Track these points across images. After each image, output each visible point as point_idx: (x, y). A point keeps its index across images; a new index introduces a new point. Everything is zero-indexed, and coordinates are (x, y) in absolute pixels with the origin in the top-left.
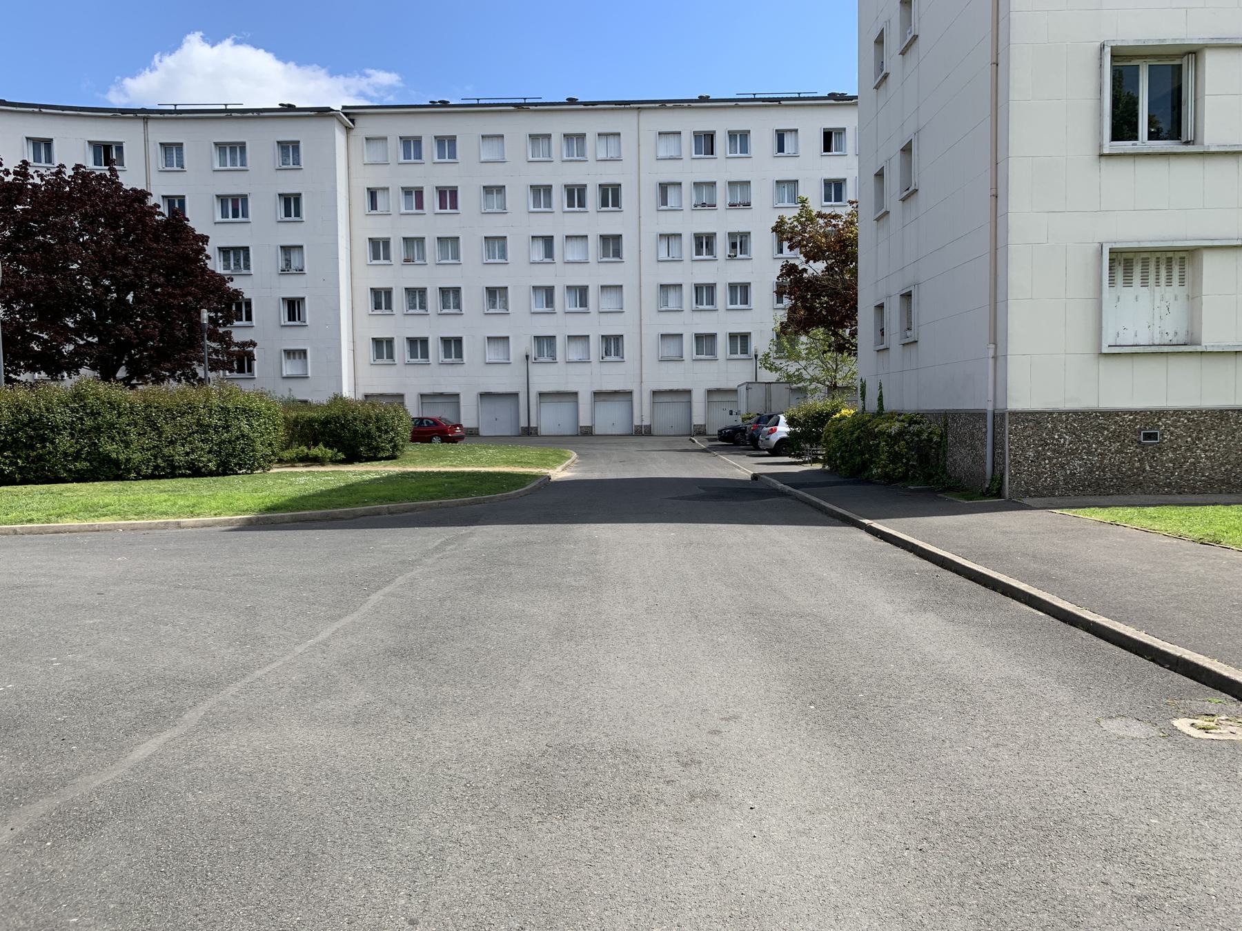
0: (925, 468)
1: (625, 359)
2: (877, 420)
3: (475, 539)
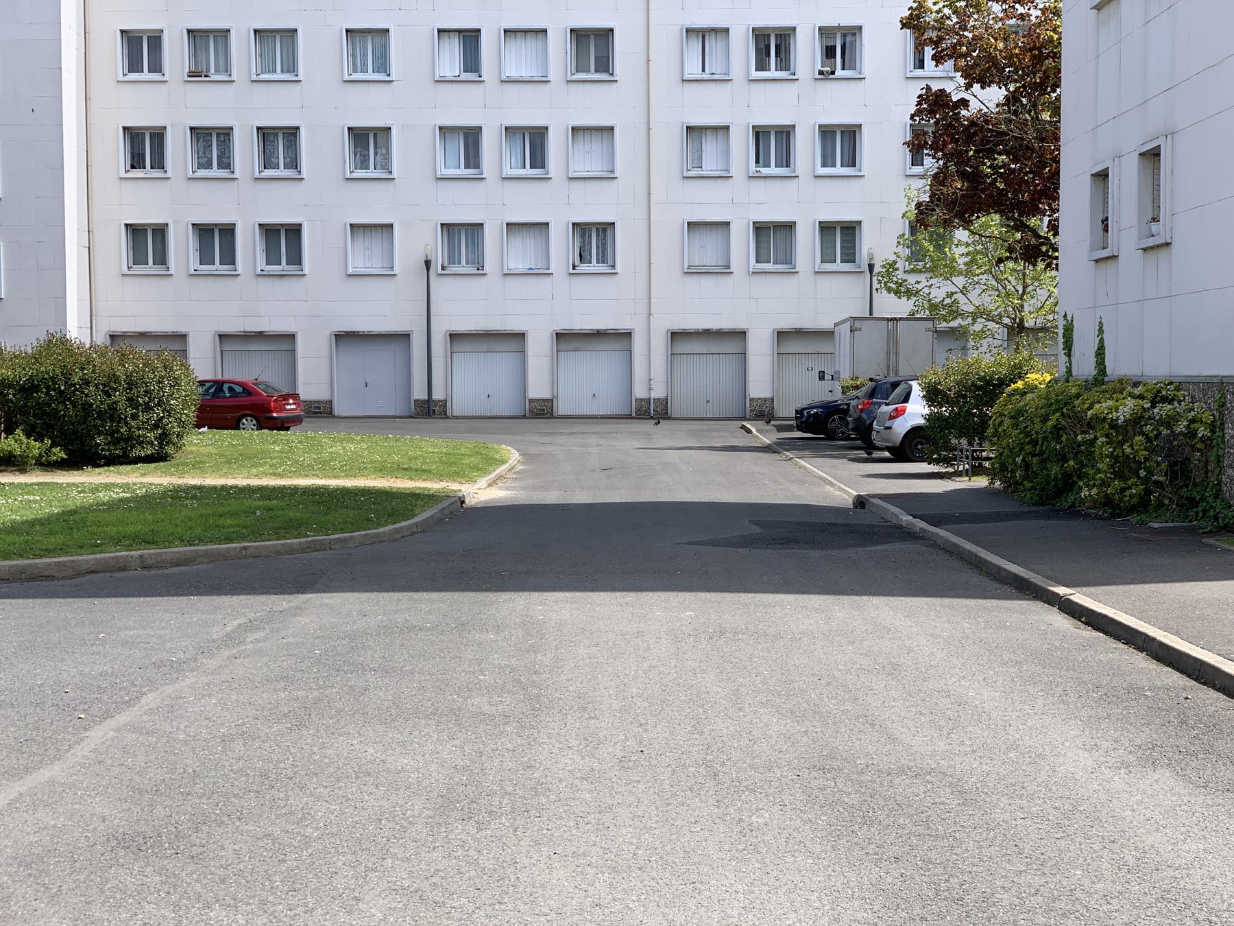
0: (1182, 487)
1: (619, 268)
2: (1094, 394)
3: (303, 620)
